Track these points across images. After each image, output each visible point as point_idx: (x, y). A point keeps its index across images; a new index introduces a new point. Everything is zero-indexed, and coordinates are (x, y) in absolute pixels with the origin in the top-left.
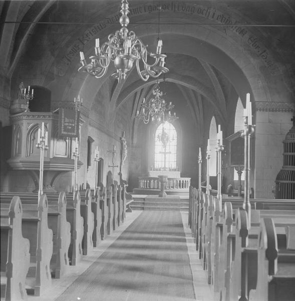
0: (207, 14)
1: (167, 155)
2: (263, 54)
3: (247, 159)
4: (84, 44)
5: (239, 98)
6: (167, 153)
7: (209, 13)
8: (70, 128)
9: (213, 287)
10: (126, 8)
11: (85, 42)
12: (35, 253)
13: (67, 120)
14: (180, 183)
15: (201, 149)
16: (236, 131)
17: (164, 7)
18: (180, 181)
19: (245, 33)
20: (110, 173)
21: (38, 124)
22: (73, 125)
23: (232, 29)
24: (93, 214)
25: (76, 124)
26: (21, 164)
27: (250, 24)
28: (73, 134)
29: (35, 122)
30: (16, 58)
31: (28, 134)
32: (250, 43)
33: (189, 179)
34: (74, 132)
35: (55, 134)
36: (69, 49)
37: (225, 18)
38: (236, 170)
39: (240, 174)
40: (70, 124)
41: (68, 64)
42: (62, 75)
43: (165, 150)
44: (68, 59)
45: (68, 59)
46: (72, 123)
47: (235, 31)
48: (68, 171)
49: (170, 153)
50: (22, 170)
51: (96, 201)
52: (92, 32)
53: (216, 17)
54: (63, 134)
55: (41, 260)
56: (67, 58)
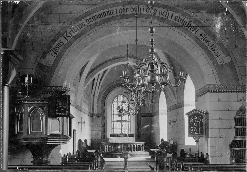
3: (204, 133)
8: (63, 109)
9: (180, 148)
15: (32, 78)
17: (132, 9)
18: (136, 145)
22: (65, 107)
23: (186, 28)
28: (65, 114)
32: (202, 39)
34: (66, 113)
37: (181, 19)
40: (63, 107)
41: (55, 57)
43: (122, 118)
44: (54, 52)
45: (54, 52)
46: (64, 105)
48: (59, 144)
52: (73, 30)
53: (174, 17)
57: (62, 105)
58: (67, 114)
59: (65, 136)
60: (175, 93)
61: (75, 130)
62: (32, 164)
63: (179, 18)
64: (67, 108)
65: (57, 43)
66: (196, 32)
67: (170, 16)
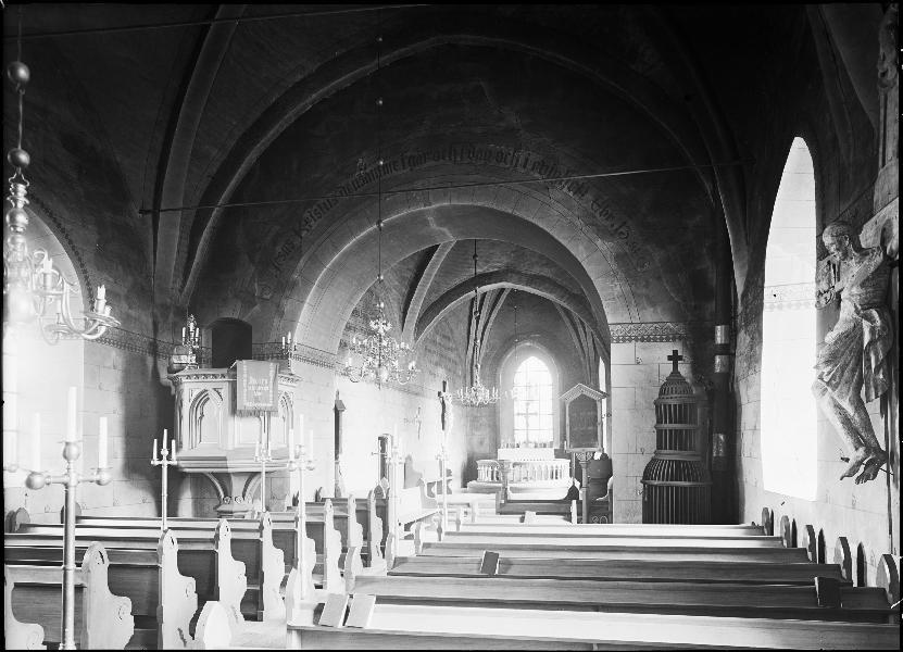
0: (514, 162)
1: (531, 418)
2: (621, 230)
7: (518, 161)
10: (20, 194)
11: (304, 234)
13: (253, 381)
19: (586, 192)
25: (271, 387)
27: (593, 172)
31: (193, 405)
36: (278, 249)
42: (268, 297)
47: (565, 190)
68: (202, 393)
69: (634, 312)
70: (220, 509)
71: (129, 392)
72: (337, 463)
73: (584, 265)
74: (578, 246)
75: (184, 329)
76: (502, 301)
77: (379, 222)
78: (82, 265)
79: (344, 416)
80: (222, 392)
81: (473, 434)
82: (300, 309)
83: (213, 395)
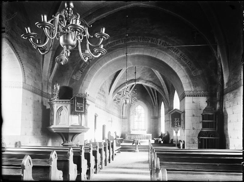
0: (157, 42)
4: (90, 62)
5: (176, 92)
6: (140, 121)
9: (171, 138)
12: (89, 165)
13: (78, 104)
14: (148, 137)
16: (174, 109)
18: (146, 136)
20: (109, 132)
21: (62, 106)
22: (82, 106)
24: (94, 157)
26: (53, 129)
28: (82, 111)
29: (61, 105)
30: (54, 69)
33: (151, 135)
35: (73, 112)
38: (175, 130)
39: (177, 132)
46: (81, 105)
49: (141, 121)
50: (54, 132)
51: (97, 149)
54: (76, 112)
55: (81, 172)
56: (80, 70)
57: (79, 105)
58: (83, 112)
59: (83, 126)
60: (169, 102)
61: (105, 125)
62: (62, 146)
63: (165, 44)
64: (83, 107)
65: (82, 64)
66: (177, 53)
67: (159, 42)
68: (61, 107)
69: (192, 87)
70: (64, 144)
71: (34, 107)
72: (95, 132)
73: (178, 73)
74: (176, 67)
75: (55, 86)
76: (133, 88)
77: (168, 37)
78: (22, 65)
79: (97, 118)
80: (68, 107)
81: (123, 126)
82: (89, 84)
83: (64, 108)
